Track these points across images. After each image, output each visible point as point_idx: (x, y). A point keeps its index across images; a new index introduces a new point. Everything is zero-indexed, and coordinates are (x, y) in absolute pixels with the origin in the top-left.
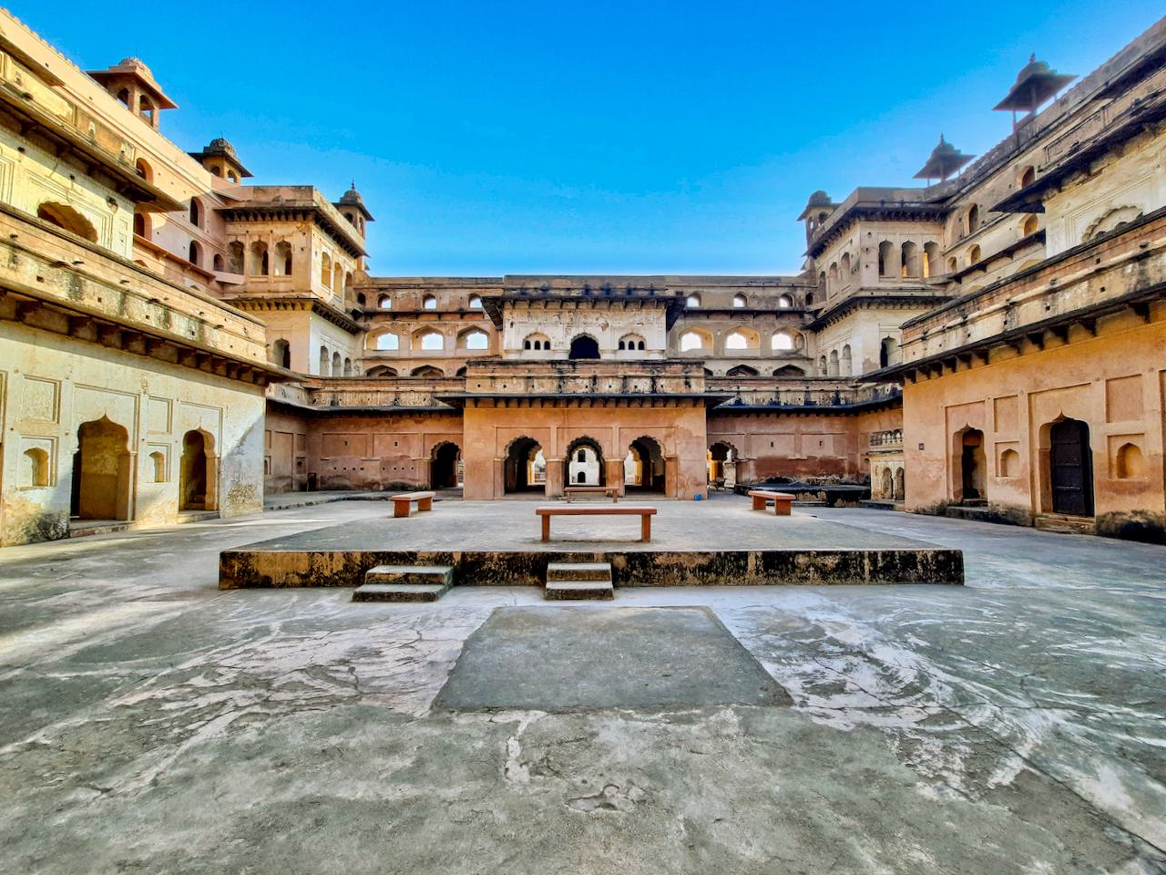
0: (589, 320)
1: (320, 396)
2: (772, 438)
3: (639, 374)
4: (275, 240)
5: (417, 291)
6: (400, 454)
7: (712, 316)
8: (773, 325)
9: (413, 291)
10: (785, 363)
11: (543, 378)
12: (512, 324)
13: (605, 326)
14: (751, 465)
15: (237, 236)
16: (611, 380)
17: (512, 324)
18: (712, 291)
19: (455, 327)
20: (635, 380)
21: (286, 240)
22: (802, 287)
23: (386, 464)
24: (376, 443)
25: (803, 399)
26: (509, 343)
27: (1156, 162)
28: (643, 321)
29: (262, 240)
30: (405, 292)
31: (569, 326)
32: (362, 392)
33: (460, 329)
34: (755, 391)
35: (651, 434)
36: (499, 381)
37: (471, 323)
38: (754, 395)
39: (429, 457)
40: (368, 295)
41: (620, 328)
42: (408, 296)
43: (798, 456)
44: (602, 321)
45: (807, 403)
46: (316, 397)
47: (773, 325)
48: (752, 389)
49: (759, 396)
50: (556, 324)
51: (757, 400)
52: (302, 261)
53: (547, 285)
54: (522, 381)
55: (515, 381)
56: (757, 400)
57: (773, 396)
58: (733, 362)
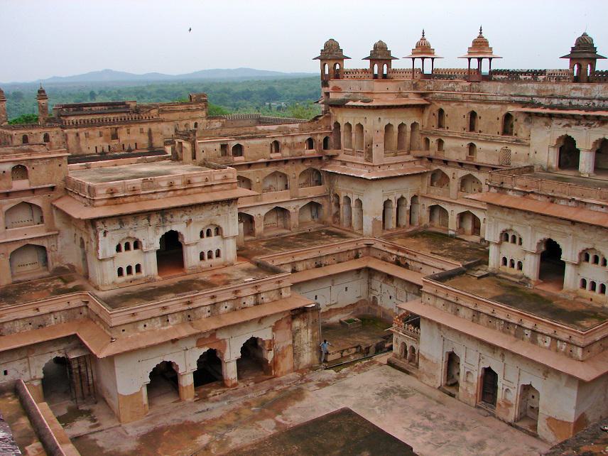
12: (105, 233)
17: (105, 233)
27: (528, 223)
41: (201, 221)
44: (186, 218)
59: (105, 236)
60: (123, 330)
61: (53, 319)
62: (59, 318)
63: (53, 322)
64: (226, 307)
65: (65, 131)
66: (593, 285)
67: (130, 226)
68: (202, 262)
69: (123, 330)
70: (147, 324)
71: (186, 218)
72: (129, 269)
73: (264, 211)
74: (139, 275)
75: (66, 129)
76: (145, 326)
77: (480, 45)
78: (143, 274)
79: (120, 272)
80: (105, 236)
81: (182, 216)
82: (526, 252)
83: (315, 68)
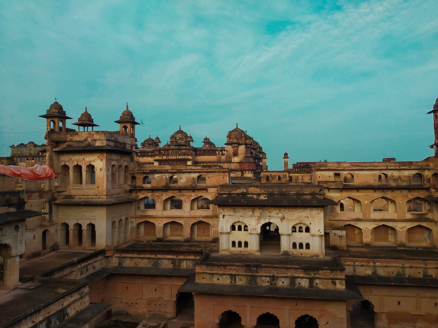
0: (272, 214)
1: (112, 259)
2: (399, 299)
3: (302, 275)
4: (85, 163)
5: (166, 175)
6: (158, 296)
7: (360, 191)
8: (407, 196)
9: (164, 174)
10: (416, 224)
11: (241, 275)
12: (224, 216)
13: (283, 219)
14: (384, 316)
15: (65, 161)
16: (283, 279)
17: (224, 216)
18: (361, 172)
19: (189, 197)
20: (300, 279)
21: (92, 164)
22: (429, 170)
23: (149, 302)
24: (144, 289)
25: (422, 273)
26: (222, 228)
28: (308, 215)
29: (79, 164)
30: (159, 175)
31: (259, 218)
32: (136, 258)
33: (193, 198)
34: (386, 266)
35: (310, 314)
36: (215, 276)
37: (200, 194)
38: (386, 269)
39: (175, 299)
40: (138, 176)
41: (293, 220)
42: (161, 178)
43: (419, 313)
44: (280, 215)
45: (425, 275)
46: (110, 260)
47: (407, 196)
48: (385, 264)
49: (390, 270)
50: (251, 216)
51: (388, 272)
52: (101, 177)
53: (245, 191)
54: (228, 277)
55: (224, 277)
56: (388, 272)
57: (400, 270)
58: (377, 223)
59: (223, 218)
60: (203, 278)
61: (185, 264)
62: (188, 264)
63: (185, 266)
64: (283, 282)
65: (291, 175)
66: (240, 243)
67: (241, 214)
68: (294, 250)
69: (203, 278)
70: (220, 278)
71: (280, 215)
72: (240, 243)
73: (371, 226)
74: (246, 249)
75: (291, 173)
76: (218, 279)
77: (128, 120)
78: (249, 248)
79: (234, 243)
80: (223, 218)
81: (277, 214)
82: (313, 235)
83: (43, 126)
